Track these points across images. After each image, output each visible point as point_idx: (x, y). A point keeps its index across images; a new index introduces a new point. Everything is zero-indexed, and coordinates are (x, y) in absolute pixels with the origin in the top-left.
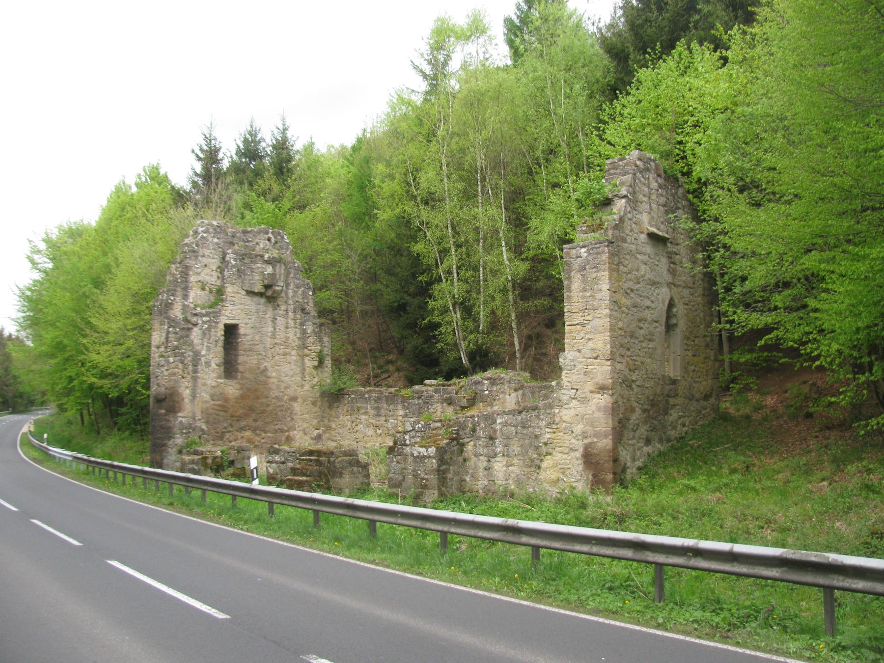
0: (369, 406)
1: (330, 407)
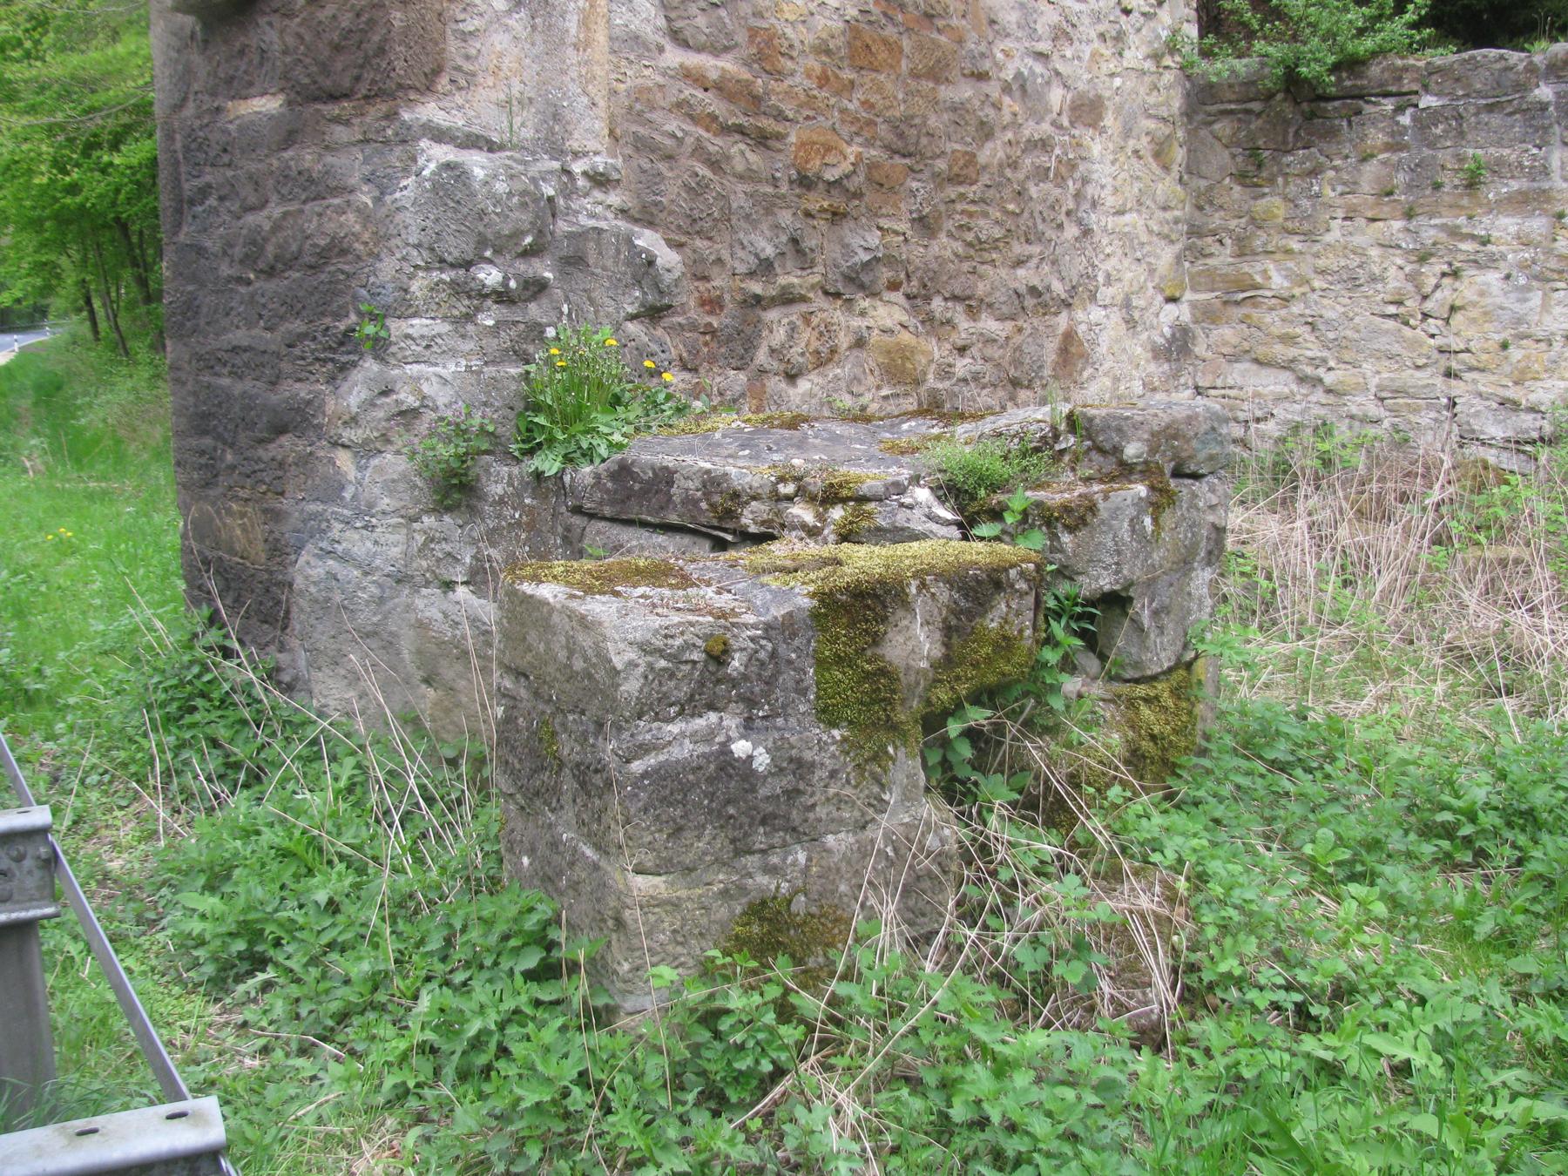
1: (1253, 171)
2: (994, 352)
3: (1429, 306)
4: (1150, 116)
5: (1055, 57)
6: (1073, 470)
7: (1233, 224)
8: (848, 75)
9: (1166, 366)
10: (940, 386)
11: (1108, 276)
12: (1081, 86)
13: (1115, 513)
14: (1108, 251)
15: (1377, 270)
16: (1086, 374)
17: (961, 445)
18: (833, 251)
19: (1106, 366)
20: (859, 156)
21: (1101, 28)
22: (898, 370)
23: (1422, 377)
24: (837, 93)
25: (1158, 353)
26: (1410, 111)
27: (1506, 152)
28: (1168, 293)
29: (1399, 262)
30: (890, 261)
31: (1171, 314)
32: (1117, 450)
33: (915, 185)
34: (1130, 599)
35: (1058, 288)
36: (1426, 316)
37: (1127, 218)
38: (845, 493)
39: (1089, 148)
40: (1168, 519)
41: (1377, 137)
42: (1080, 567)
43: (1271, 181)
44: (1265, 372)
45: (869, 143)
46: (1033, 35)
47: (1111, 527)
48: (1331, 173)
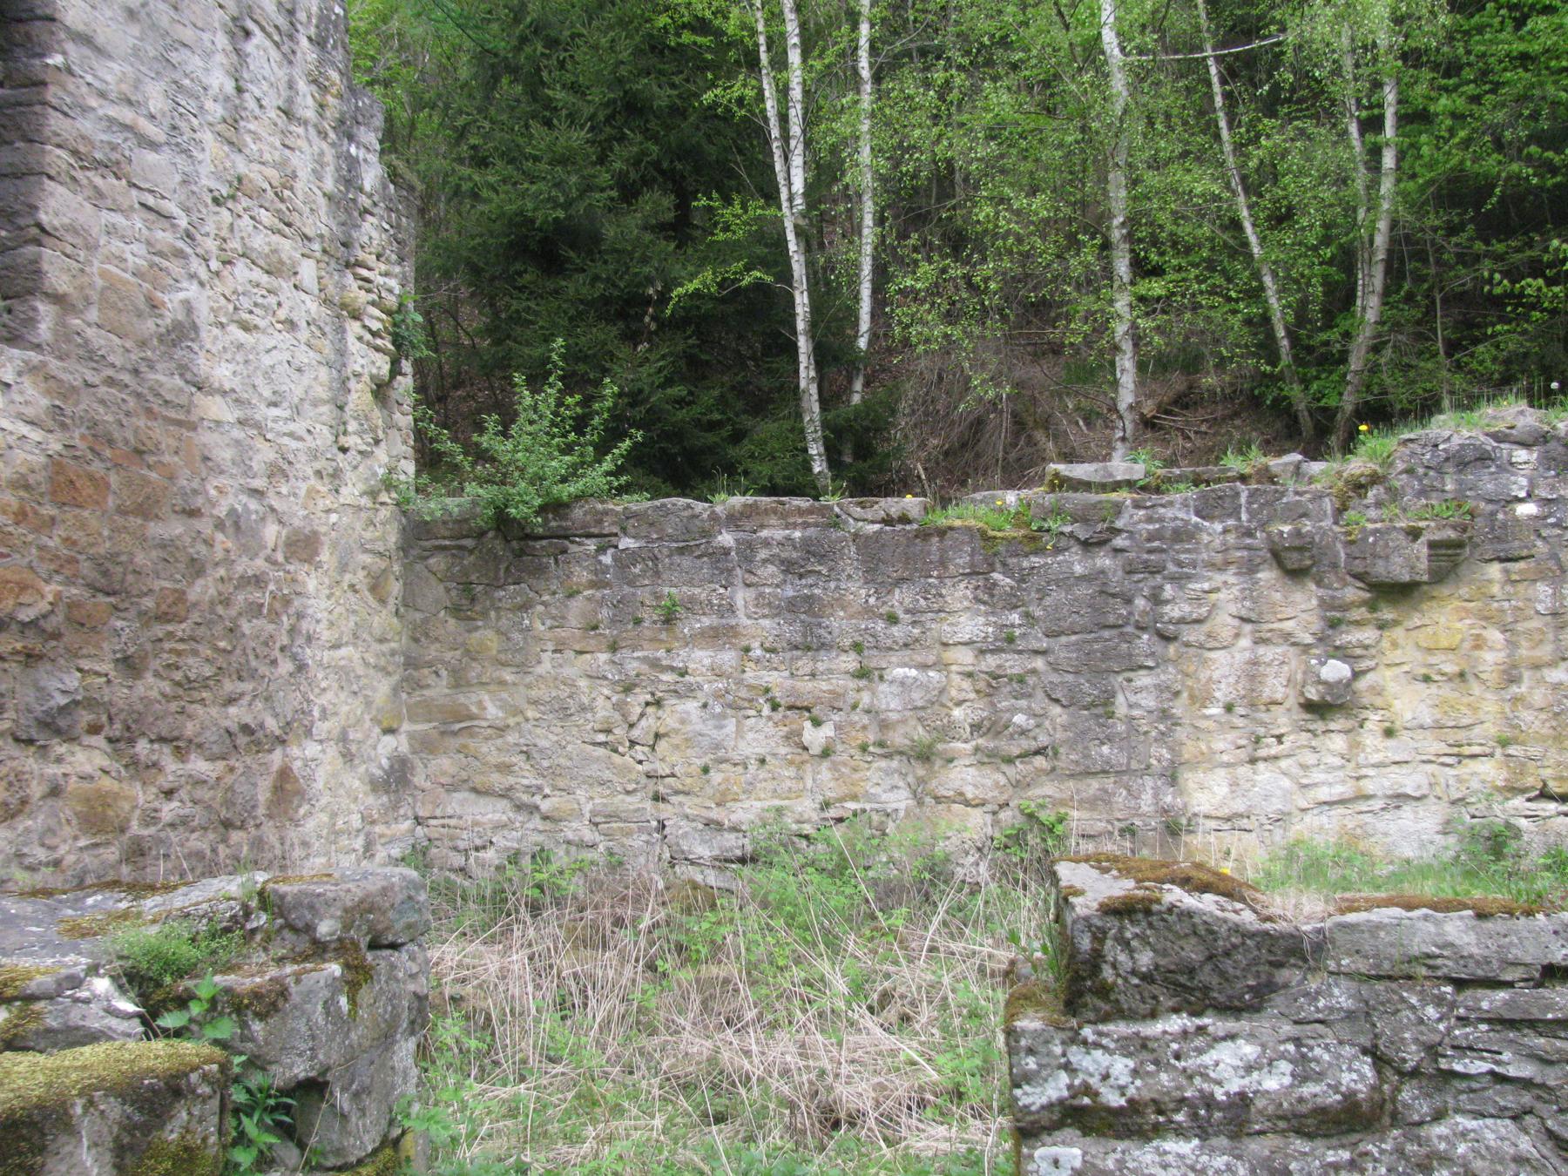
0: (742, 597)
2: (204, 794)
3: (635, 733)
4: (366, 551)
5: (271, 493)
6: (266, 949)
7: (448, 656)
8: (48, 510)
9: (385, 799)
10: (146, 832)
11: (324, 711)
12: (297, 523)
13: (308, 995)
14: (324, 684)
15: (586, 701)
16: (302, 811)
17: (150, 924)
18: (28, 696)
19: (324, 801)
20: (58, 595)
21: (318, 465)
22: (98, 818)
23: (633, 802)
24: (37, 530)
25: (377, 786)
26: (611, 551)
27: (697, 591)
28: (385, 724)
29: (606, 692)
30: (90, 703)
31: (388, 746)
32: (309, 929)
33: (119, 624)
34: (326, 1083)
35: (272, 724)
36: (633, 743)
37: (343, 652)
38: (9, 992)
39: (304, 584)
40: (365, 995)
41: (581, 575)
42: (272, 1055)
43: (484, 614)
44: (482, 801)
45: (69, 582)
46: (248, 472)
47: (303, 1012)
48: (540, 608)
